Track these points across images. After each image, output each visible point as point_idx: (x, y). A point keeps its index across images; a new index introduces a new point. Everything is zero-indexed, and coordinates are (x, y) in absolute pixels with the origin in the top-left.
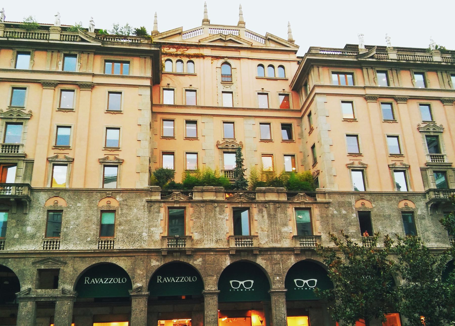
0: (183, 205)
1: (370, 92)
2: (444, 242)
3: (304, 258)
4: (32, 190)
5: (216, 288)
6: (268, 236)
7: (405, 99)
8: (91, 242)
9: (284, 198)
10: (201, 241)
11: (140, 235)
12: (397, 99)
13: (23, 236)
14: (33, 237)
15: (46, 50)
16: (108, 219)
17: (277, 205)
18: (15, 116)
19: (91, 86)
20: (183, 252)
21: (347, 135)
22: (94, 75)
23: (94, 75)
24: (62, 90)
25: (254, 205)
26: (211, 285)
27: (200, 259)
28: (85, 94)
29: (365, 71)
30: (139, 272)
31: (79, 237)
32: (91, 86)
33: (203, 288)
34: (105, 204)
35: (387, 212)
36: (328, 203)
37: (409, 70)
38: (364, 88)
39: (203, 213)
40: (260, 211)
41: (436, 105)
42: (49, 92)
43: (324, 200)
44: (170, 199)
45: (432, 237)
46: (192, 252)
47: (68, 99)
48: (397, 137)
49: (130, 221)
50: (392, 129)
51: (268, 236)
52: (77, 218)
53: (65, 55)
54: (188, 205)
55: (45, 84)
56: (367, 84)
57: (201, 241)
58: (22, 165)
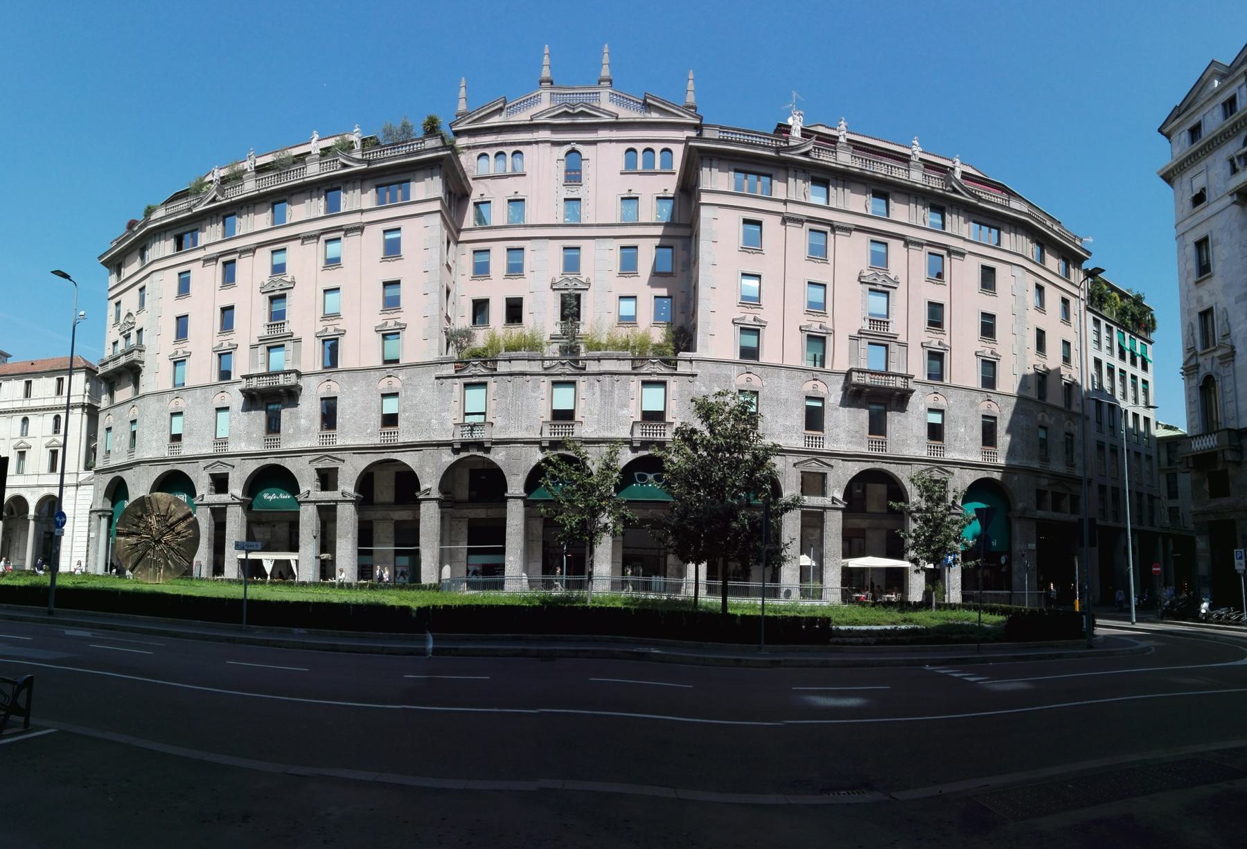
0: (483, 379)
1: (793, 209)
2: (860, 444)
3: (646, 453)
4: (299, 375)
5: (522, 490)
6: (599, 422)
7: (848, 230)
8: (371, 435)
9: (626, 366)
10: (505, 428)
11: (429, 422)
12: (835, 228)
13: (297, 428)
14: (307, 431)
15: (303, 192)
16: (390, 406)
17: (616, 377)
18: (277, 287)
19: (359, 229)
20: (479, 445)
21: (743, 274)
22: (362, 211)
23: (362, 211)
24: (327, 241)
25: (582, 378)
26: (516, 486)
27: (504, 453)
28: (354, 239)
29: (791, 180)
30: (428, 470)
31: (358, 428)
32: (359, 229)
33: (506, 491)
34: (386, 386)
35: (784, 394)
36: (694, 375)
37: (865, 184)
38: (785, 202)
39: (510, 391)
40: (591, 386)
41: (896, 246)
42: (311, 246)
43: (688, 371)
44: (466, 373)
45: (843, 435)
46: (493, 443)
47: (333, 249)
48: (825, 286)
49: (416, 405)
50: (819, 272)
51: (599, 422)
52: (354, 406)
53: (327, 191)
54: (490, 380)
55: (305, 238)
56: (792, 197)
57: (505, 428)
58: (289, 345)
